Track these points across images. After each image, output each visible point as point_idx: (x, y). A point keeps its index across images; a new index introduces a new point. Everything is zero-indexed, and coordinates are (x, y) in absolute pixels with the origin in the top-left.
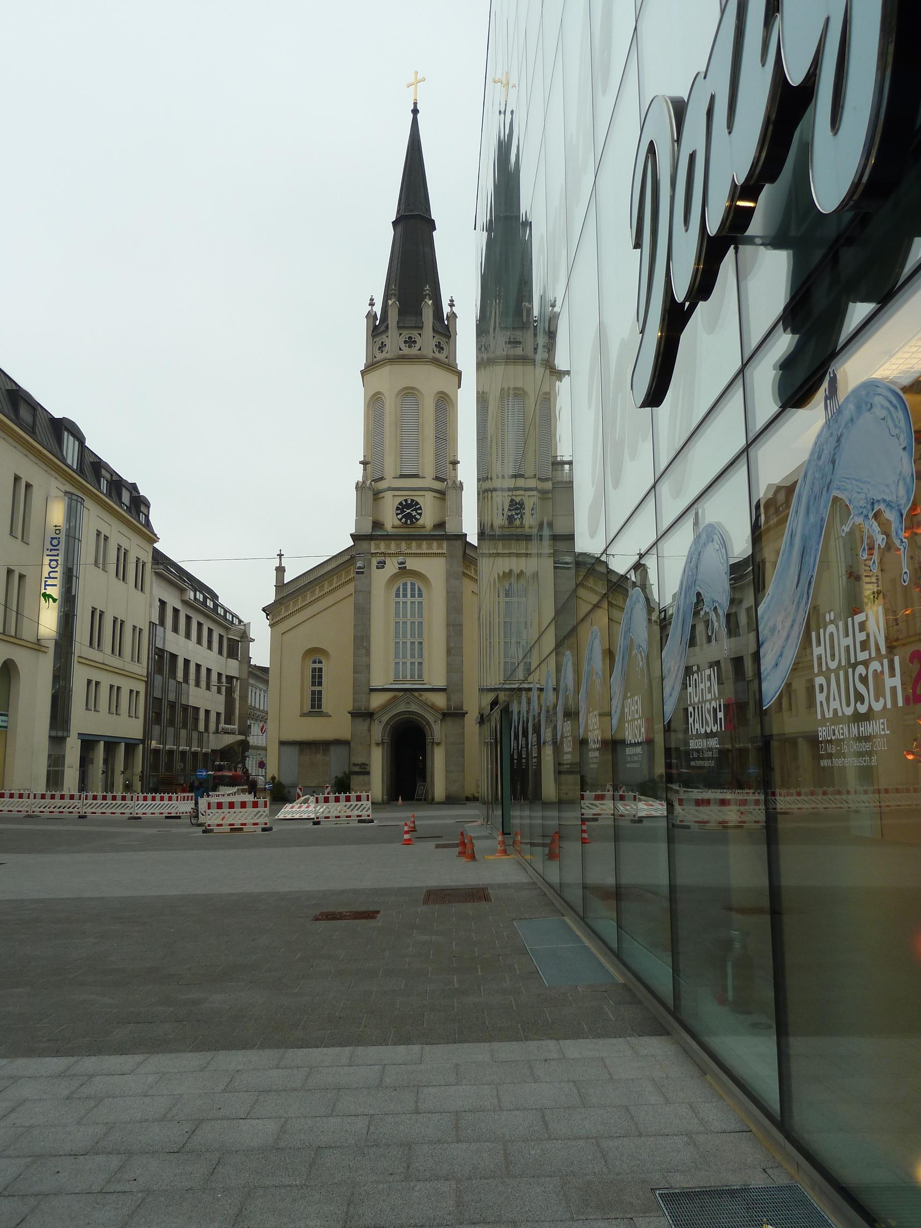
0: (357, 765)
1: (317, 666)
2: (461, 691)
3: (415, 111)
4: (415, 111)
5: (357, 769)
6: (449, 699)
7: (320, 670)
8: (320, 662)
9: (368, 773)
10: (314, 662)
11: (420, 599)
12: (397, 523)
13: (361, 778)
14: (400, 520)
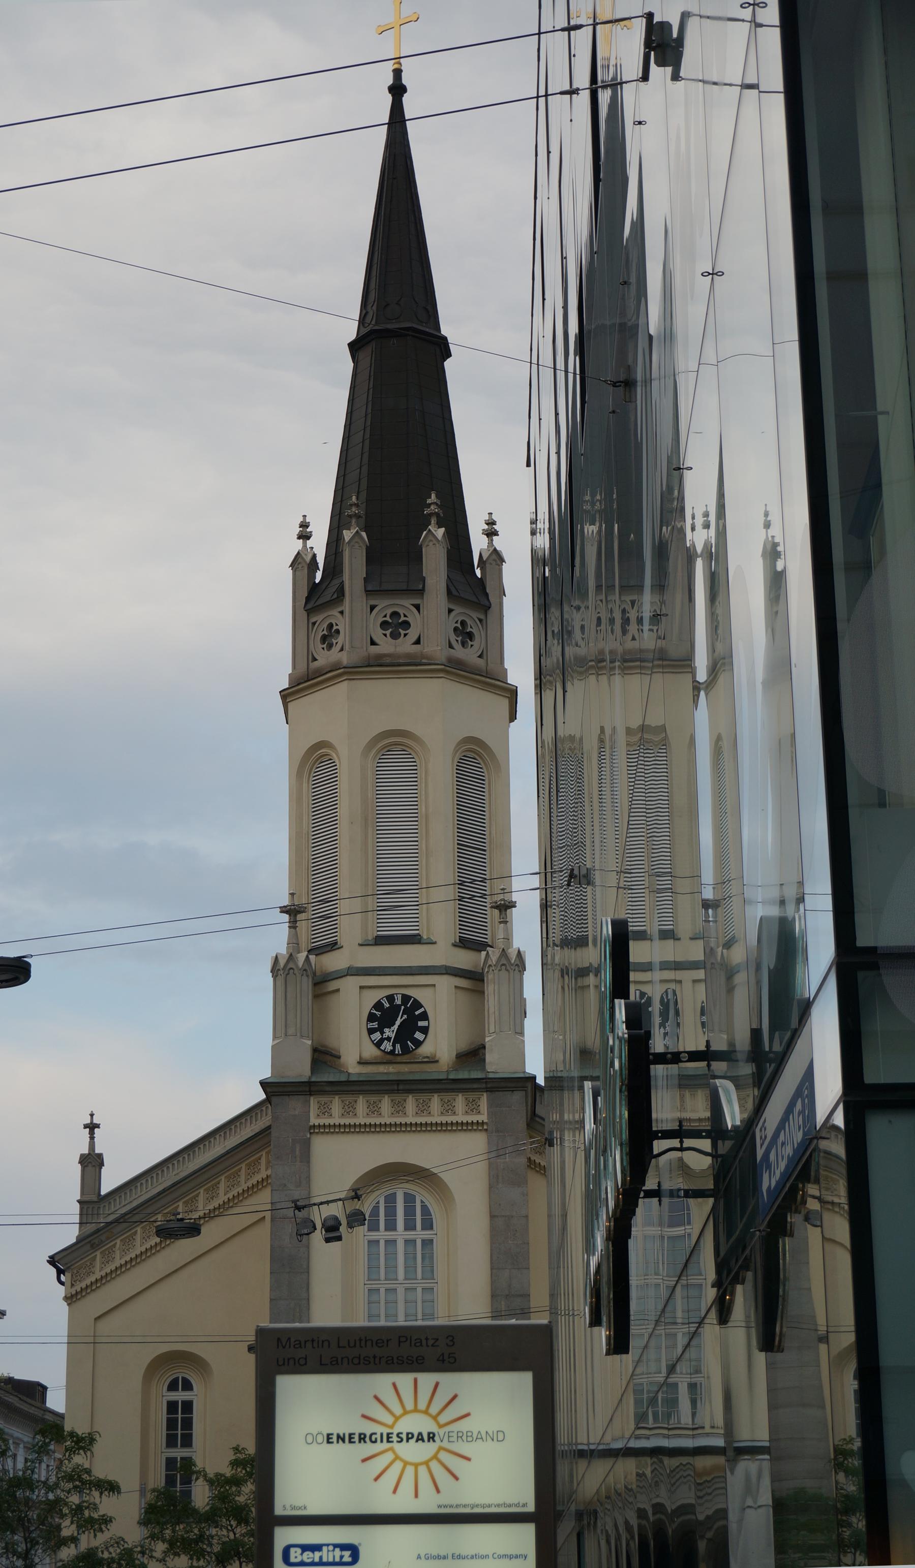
1: (180, 1396)
4: (398, 90)
7: (188, 1406)
8: (188, 1386)
10: (173, 1386)
11: (427, 1235)
12: (371, 1051)
14: (378, 1044)
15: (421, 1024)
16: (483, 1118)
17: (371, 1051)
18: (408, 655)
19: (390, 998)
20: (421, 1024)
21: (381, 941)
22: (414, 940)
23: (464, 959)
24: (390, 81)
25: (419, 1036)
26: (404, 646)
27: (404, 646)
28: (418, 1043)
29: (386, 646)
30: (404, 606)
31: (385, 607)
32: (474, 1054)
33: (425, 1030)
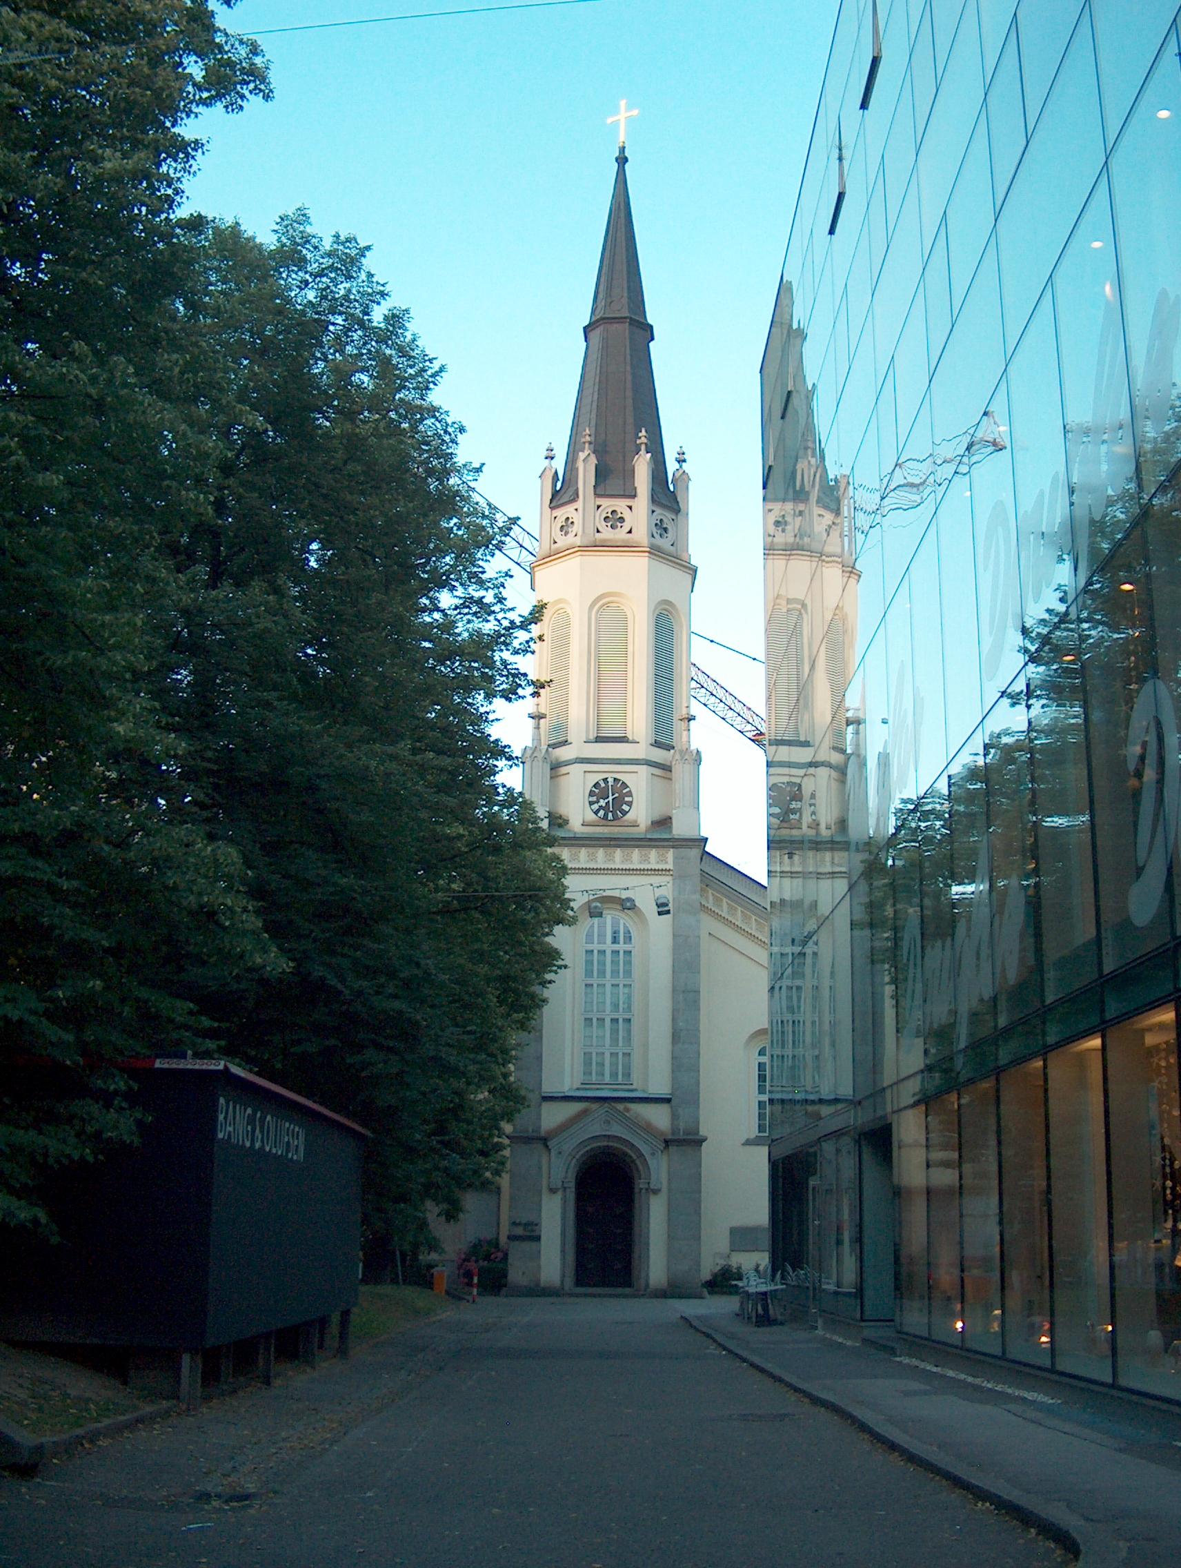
0: (520, 1224)
2: (695, 1102)
3: (622, 160)
4: (622, 160)
5: (519, 1231)
6: (674, 1116)
9: (538, 1238)
12: (591, 817)
13: (526, 1246)
14: (596, 813)
15: (627, 799)
16: (670, 866)
17: (591, 817)
18: (623, 541)
19: (605, 780)
20: (627, 799)
21: (599, 740)
22: (623, 740)
23: (659, 755)
24: (617, 154)
25: (625, 807)
26: (620, 534)
27: (620, 534)
28: (625, 813)
29: (607, 534)
30: (620, 505)
31: (608, 504)
32: (664, 822)
33: (630, 804)
